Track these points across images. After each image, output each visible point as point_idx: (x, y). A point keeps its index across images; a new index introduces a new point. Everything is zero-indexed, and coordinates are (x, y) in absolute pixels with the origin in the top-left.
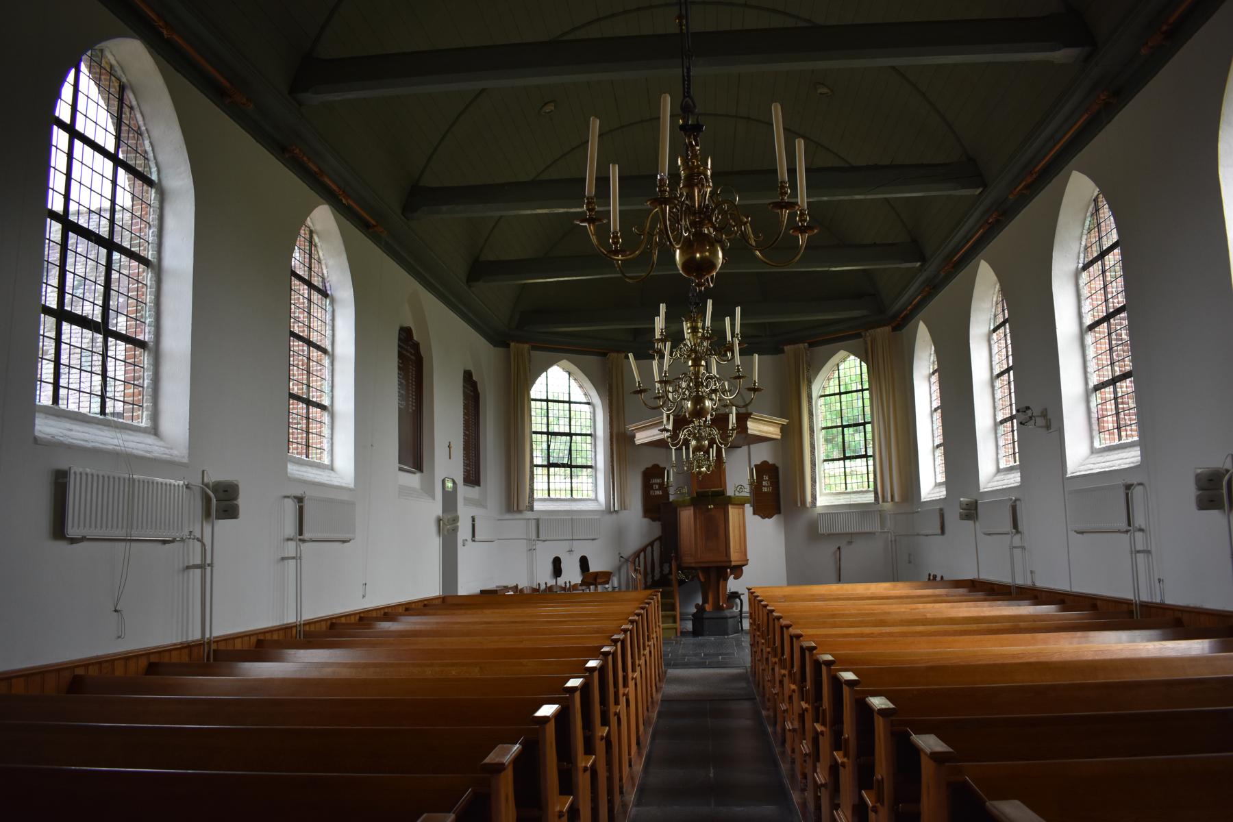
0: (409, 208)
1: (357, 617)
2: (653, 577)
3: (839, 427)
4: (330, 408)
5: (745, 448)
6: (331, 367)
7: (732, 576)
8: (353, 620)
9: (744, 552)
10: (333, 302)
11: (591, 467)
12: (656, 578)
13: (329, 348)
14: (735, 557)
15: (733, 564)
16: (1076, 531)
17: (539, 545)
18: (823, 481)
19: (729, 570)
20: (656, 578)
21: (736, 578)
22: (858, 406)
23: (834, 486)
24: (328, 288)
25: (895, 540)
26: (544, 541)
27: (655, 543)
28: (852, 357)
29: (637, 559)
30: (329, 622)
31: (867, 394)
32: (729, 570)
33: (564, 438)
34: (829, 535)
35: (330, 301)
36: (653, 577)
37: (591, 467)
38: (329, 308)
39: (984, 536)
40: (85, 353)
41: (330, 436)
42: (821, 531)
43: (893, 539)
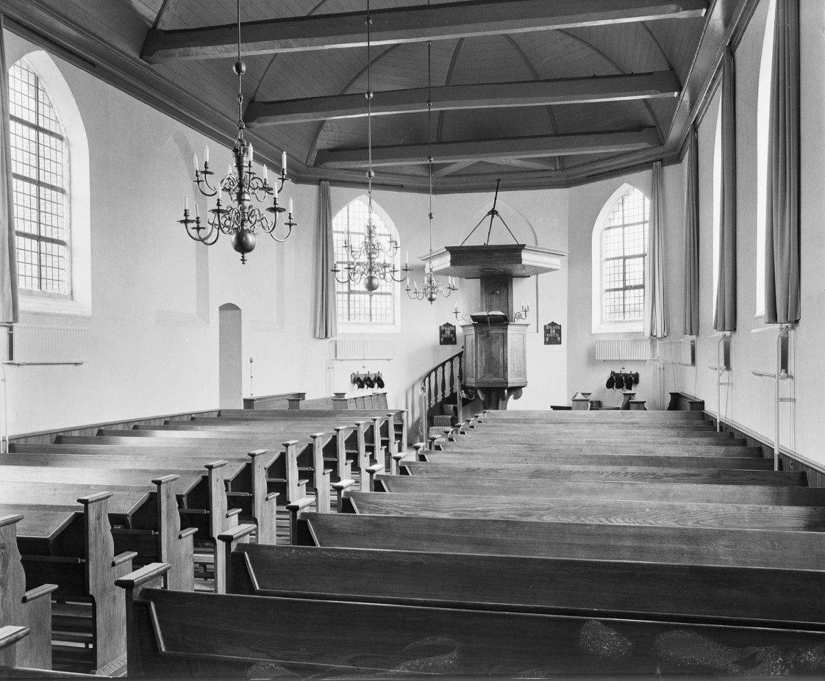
0: (145, 52)
1: (96, 431)
2: (443, 395)
3: (619, 258)
4: (68, 243)
5: (533, 278)
6: (68, 206)
7: (512, 396)
8: (185, 419)
9: (523, 373)
10: (68, 144)
11: (389, 294)
12: (446, 396)
13: (66, 188)
14: (512, 380)
15: (509, 385)
16: (753, 373)
17: (337, 365)
18: (604, 310)
19: (506, 391)
20: (446, 396)
21: (515, 398)
22: (638, 239)
23: (361, 313)
24: (63, 131)
25: (664, 368)
26: (342, 360)
27: (447, 364)
28: (636, 190)
29: (427, 379)
30: (55, 436)
31: (647, 225)
32: (506, 391)
33: (632, 283)
34: (604, 361)
35: (66, 143)
36: (436, 399)
37: (389, 294)
38: (66, 151)
39: (710, 370)
40: (54, 217)
41: (69, 269)
42: (598, 357)
43: (662, 367)
